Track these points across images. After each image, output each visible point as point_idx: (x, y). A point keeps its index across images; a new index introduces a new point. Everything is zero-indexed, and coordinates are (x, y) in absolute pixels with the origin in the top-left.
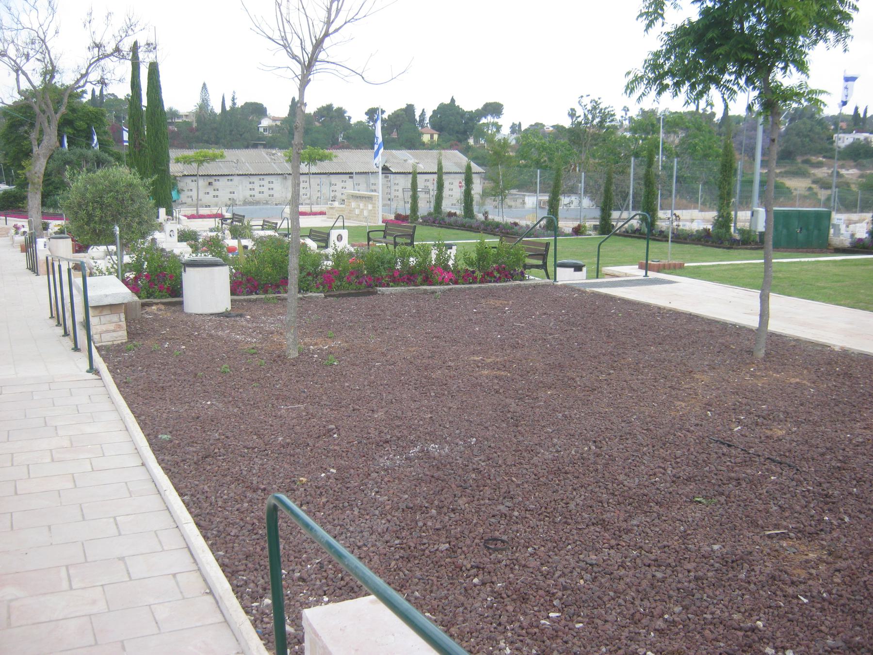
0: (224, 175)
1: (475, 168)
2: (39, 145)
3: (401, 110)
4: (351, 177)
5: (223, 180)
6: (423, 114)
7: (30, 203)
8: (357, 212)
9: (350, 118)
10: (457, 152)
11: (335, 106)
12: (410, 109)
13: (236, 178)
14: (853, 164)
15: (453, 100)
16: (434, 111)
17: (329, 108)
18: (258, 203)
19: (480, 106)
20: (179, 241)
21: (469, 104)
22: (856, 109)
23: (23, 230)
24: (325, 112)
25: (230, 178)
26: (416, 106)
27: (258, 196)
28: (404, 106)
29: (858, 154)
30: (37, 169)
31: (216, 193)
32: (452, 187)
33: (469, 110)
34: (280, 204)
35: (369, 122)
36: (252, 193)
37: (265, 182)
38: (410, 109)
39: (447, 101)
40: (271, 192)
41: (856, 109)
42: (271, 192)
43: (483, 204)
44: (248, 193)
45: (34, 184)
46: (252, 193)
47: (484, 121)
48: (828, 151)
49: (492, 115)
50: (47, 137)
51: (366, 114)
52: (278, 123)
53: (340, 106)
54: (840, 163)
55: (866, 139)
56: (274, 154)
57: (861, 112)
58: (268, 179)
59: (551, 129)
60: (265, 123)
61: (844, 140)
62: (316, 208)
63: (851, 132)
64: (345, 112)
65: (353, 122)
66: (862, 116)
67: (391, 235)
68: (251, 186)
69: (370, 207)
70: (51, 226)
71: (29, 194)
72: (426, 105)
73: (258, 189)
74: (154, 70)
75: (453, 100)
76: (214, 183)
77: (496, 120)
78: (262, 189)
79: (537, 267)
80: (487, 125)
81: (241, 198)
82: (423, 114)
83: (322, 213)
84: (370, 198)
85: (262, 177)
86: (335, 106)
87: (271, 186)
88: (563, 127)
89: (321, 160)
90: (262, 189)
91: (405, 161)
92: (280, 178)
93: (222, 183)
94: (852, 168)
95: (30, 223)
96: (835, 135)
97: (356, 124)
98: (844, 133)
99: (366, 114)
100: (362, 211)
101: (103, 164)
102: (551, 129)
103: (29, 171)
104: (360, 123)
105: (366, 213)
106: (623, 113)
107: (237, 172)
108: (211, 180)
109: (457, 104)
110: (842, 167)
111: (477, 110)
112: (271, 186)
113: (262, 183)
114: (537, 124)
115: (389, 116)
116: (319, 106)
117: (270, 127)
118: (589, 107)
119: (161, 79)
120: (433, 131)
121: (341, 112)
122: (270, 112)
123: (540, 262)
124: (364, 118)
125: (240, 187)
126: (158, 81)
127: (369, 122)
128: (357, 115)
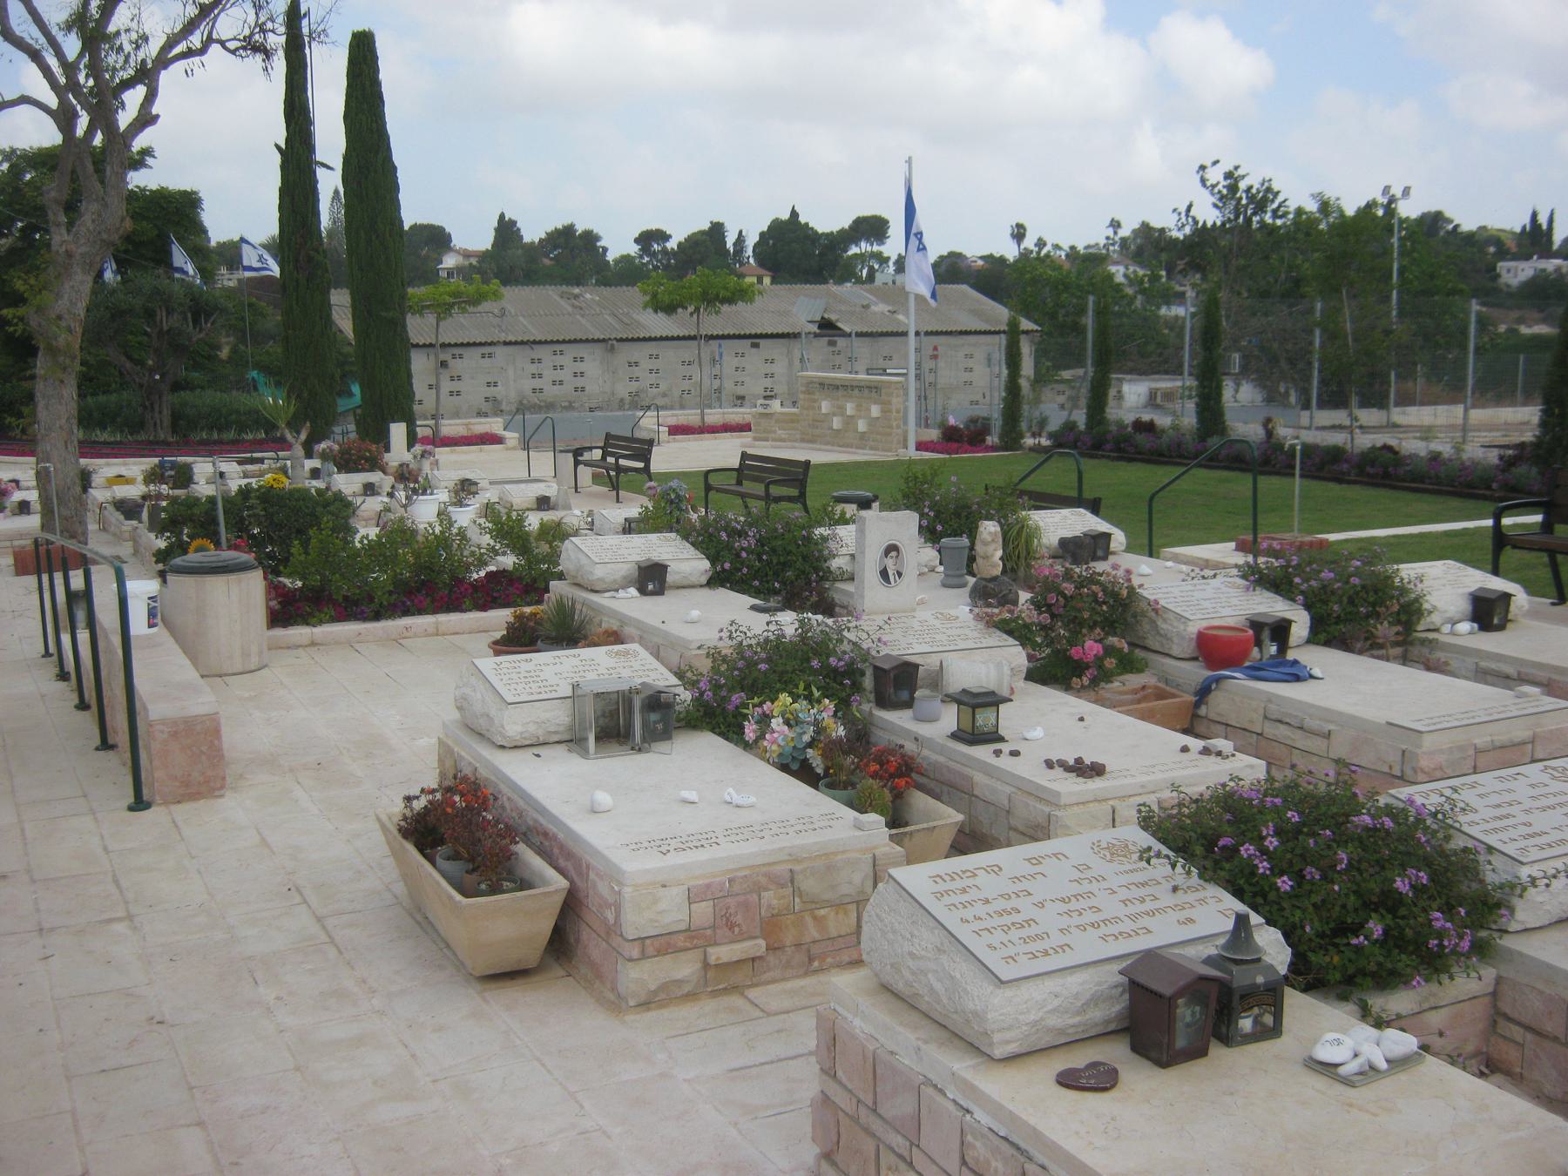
0: (475, 344)
1: (1026, 324)
2: (70, 225)
3: (702, 233)
4: (755, 346)
5: (472, 358)
6: (740, 239)
7: (42, 414)
8: (837, 423)
9: (605, 250)
10: (965, 287)
11: (580, 228)
12: (717, 230)
13: (500, 351)
14: (1537, 315)
15: (794, 214)
16: (762, 235)
17: (568, 231)
18: (550, 406)
19: (845, 223)
20: (666, 567)
21: (826, 219)
22: (1534, 215)
23: (17, 496)
24: (562, 240)
25: (487, 350)
26: (728, 226)
27: (551, 392)
28: (706, 226)
29: (1539, 293)
30: (62, 305)
31: (455, 386)
32: (970, 363)
33: (827, 230)
34: (599, 408)
35: (641, 257)
36: (537, 383)
37: (566, 360)
38: (717, 230)
39: (785, 215)
40: (580, 382)
41: (1534, 215)
42: (580, 382)
43: (1037, 401)
44: (528, 385)
45: (53, 351)
46: (537, 383)
47: (854, 250)
48: (1490, 291)
49: (868, 240)
50: (94, 207)
51: (637, 241)
52: (474, 261)
53: (589, 227)
54: (1515, 314)
55: (1558, 269)
56: (576, 297)
57: (1543, 220)
58: (572, 351)
59: (980, 263)
60: (450, 261)
61: (1516, 273)
62: (714, 416)
63: (1528, 258)
64: (598, 238)
65: (610, 257)
66: (1544, 227)
67: (612, 454)
68: (533, 368)
69: (875, 411)
70: (97, 480)
71: (40, 387)
72: (747, 223)
73: (549, 375)
74: (363, 51)
75: (794, 214)
76: (451, 363)
77: (876, 248)
78: (560, 375)
79: (790, 499)
80: (861, 257)
81: (513, 395)
82: (740, 239)
83: (745, 428)
84: (874, 388)
85: (558, 347)
86: (580, 228)
87: (581, 367)
88: (1002, 260)
89: (730, 301)
90: (560, 375)
91: (866, 307)
92: (598, 349)
93: (469, 363)
94: (1537, 322)
95: (42, 477)
96: (1500, 264)
97: (617, 261)
98: (1513, 259)
99: (637, 241)
100: (850, 421)
101: (208, 315)
102: (980, 263)
103: (40, 310)
104: (626, 259)
105: (862, 426)
106: (1110, 232)
107: (503, 337)
108: (445, 356)
109: (802, 219)
110: (1521, 321)
111: (842, 231)
112: (581, 367)
113: (559, 360)
114: (952, 255)
115: (680, 245)
116: (550, 229)
117: (460, 269)
118: (1222, 187)
119: (381, 76)
120: (761, 271)
121: (590, 238)
122: (457, 242)
123: (794, 492)
124: (633, 249)
125: (511, 372)
126: (376, 84)
127: (641, 257)
128: (619, 244)
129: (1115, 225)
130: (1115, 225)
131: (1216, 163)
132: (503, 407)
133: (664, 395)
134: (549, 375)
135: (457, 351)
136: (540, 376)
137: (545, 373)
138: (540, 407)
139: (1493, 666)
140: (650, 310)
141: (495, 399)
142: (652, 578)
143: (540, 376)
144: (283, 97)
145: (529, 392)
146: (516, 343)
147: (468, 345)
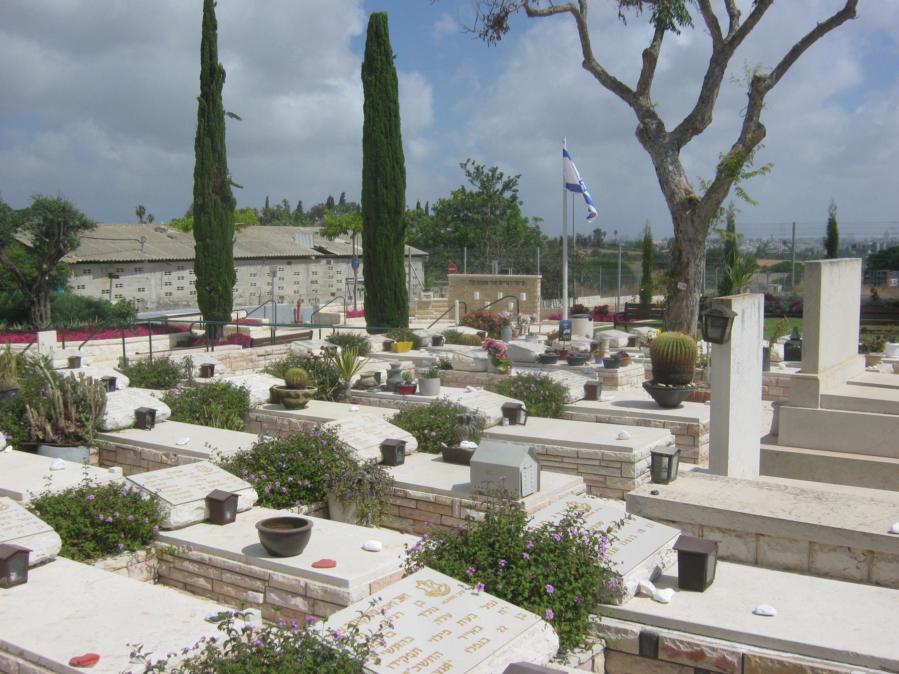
22: (418, 204)
27: (177, 294)
36: (168, 289)
46: (168, 289)
81: (154, 297)
129: (521, 203)
130: (521, 203)
131: (468, 160)
132: (149, 306)
133: (241, 297)
134: (176, 283)
135: (120, 266)
136: (170, 284)
137: (173, 282)
138: (170, 305)
139: (206, 556)
140: (602, 231)
141: (143, 300)
142: (145, 419)
143: (170, 284)
144: (200, 73)
145: (163, 295)
146: (159, 261)
147: (127, 262)
